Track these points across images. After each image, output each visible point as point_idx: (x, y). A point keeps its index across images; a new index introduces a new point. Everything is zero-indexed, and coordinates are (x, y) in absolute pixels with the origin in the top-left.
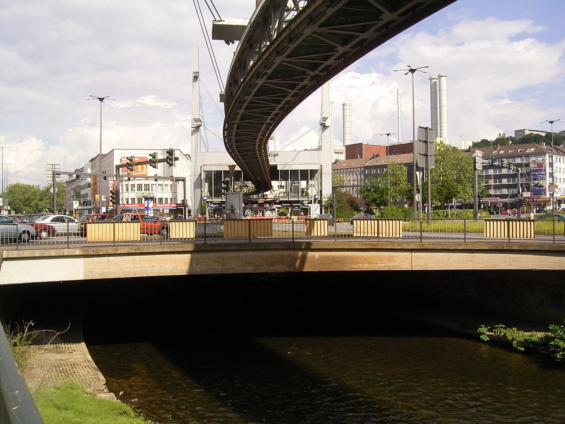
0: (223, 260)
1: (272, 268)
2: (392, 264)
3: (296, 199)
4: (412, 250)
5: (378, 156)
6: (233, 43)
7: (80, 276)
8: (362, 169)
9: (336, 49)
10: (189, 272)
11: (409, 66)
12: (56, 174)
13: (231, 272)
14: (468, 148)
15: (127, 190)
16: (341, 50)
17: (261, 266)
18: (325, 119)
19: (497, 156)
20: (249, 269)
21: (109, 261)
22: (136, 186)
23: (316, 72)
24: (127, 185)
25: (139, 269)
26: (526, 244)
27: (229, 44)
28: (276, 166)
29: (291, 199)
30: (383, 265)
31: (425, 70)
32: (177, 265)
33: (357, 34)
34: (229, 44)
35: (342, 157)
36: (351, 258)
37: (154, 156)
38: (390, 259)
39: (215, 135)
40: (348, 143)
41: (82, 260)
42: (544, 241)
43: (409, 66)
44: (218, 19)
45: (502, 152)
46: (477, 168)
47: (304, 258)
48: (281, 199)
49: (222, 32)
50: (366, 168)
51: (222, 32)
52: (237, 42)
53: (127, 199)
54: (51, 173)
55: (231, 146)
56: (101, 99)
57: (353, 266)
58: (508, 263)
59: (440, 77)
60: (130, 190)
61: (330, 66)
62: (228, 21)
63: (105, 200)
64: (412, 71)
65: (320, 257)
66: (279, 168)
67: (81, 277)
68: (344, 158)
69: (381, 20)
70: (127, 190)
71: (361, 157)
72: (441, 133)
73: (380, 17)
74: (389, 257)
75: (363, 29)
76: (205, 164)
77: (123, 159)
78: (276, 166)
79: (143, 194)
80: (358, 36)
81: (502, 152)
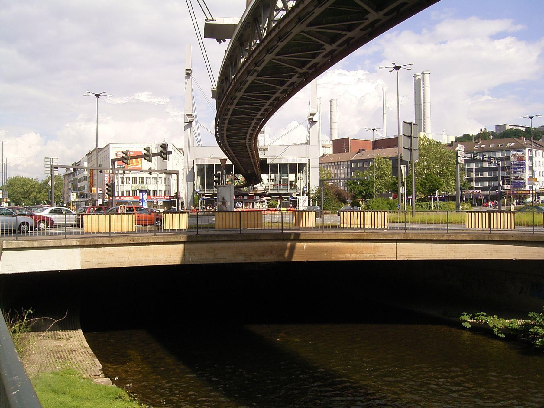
0: (214, 250)
1: (261, 258)
2: (377, 254)
3: (285, 192)
4: (396, 241)
5: (363, 150)
6: (225, 41)
7: (77, 266)
8: (349, 163)
9: (323, 47)
10: (182, 262)
11: (394, 64)
12: (54, 168)
13: (222, 261)
14: (450, 142)
15: (123, 183)
16: (328, 48)
17: (251, 256)
18: (313, 114)
19: (478, 150)
20: (240, 259)
21: (105, 252)
22: (131, 179)
23: (305, 70)
24: (122, 178)
25: (134, 259)
26: (507, 235)
27: (220, 42)
28: (265, 160)
29: (280, 192)
30: (369, 255)
31: (409, 67)
32: (170, 255)
33: (344, 33)
34: (220, 42)
35: (330, 151)
36: (338, 248)
38: (375, 250)
39: (207, 129)
40: (335, 137)
41: (79, 250)
42: (523, 232)
43: (394, 64)
44: (210, 18)
45: (483, 146)
46: (459, 161)
47: (292, 248)
48: (270, 192)
49: (214, 31)
50: (352, 161)
51: (214, 31)
52: (228, 41)
53: (123, 192)
54: (49, 166)
55: (223, 141)
56: (98, 96)
57: (340, 256)
58: (489, 253)
59: (423, 74)
60: (125, 183)
61: (318, 63)
62: (220, 20)
63: (101, 192)
64: (397, 68)
65: (308, 247)
66: (269, 162)
67: (78, 267)
68: (331, 152)
69: (367, 19)
70: (123, 183)
71: (348, 151)
72: (424, 128)
73: (366, 16)
74: (375, 247)
75: (350, 28)
76: (198, 158)
77: (118, 153)
78: (265, 160)
79: (138, 186)
80: (345, 35)
81: (483, 146)
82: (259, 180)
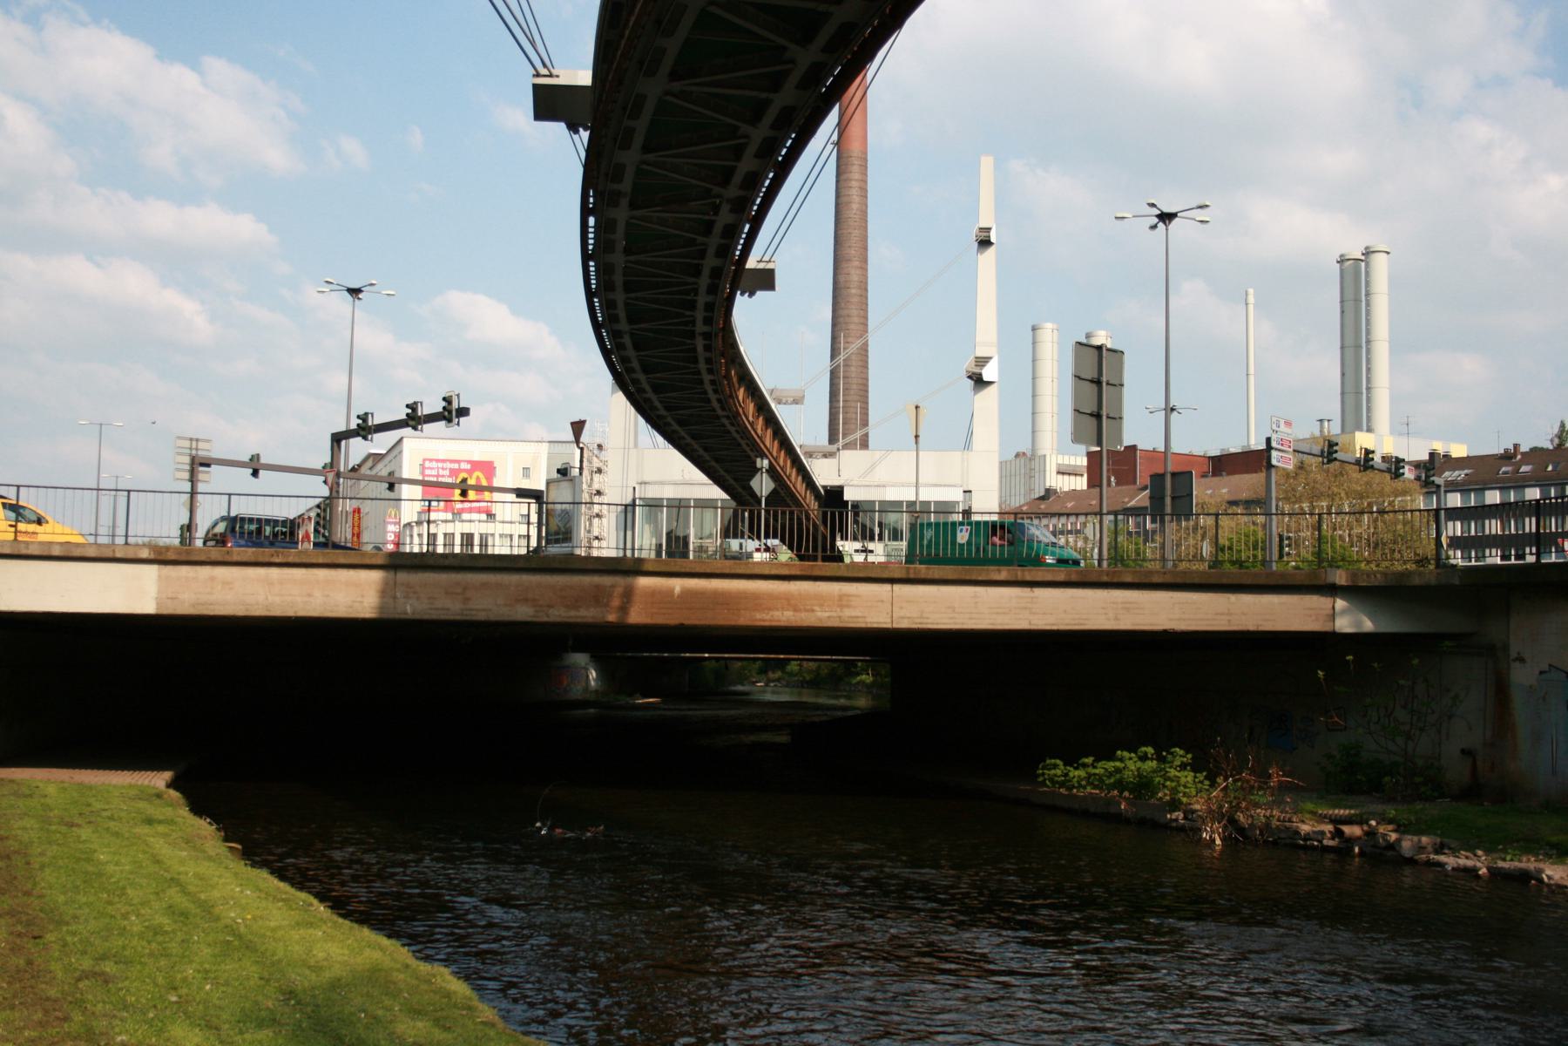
0: (465, 589)
1: (573, 613)
2: (847, 613)
4: (892, 581)
7: (147, 606)
10: (381, 608)
11: (1153, 205)
13: (482, 616)
14: (1426, 457)
17: (550, 606)
18: (982, 361)
19: (1509, 479)
20: (523, 613)
21: (212, 579)
25: (277, 599)
37: (413, 407)
38: (842, 602)
43: (1153, 205)
44: (544, 71)
45: (1524, 469)
46: (1274, 462)
54: (187, 460)
56: (355, 292)
57: (758, 616)
58: (1111, 615)
59: (1368, 252)
64: (1166, 217)
66: (849, 495)
72: (1369, 419)
74: (841, 597)
76: (646, 479)
77: (427, 464)
81: (1524, 469)
82: (1270, 776)
